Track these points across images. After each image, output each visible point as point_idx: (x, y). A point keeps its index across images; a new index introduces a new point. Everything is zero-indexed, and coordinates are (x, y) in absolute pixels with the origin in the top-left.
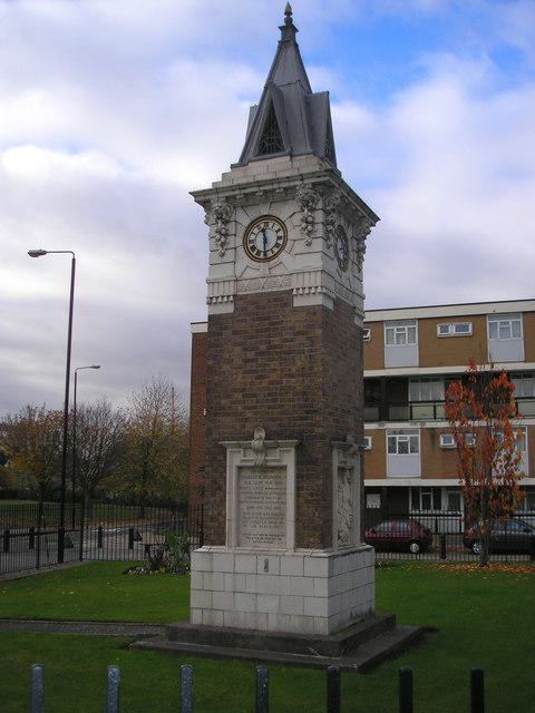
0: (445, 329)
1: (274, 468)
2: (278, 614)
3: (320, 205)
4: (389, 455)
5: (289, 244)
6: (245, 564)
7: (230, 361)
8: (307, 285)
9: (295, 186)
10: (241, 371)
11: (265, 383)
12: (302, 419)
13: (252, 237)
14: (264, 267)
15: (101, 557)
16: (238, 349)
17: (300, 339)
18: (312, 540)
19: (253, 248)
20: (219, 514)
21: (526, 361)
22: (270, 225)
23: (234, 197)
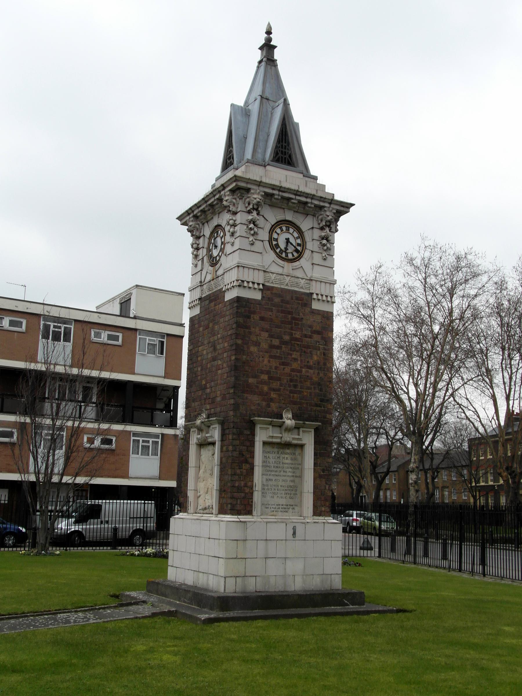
0: (98, 335)
1: (296, 446)
2: (303, 575)
4: (132, 456)
6: (278, 531)
7: (257, 344)
9: (324, 207)
10: (267, 355)
11: (287, 370)
12: (317, 405)
13: (275, 236)
14: (288, 267)
16: (265, 335)
17: (316, 337)
18: (323, 509)
19: (277, 246)
20: (246, 485)
23: (272, 195)
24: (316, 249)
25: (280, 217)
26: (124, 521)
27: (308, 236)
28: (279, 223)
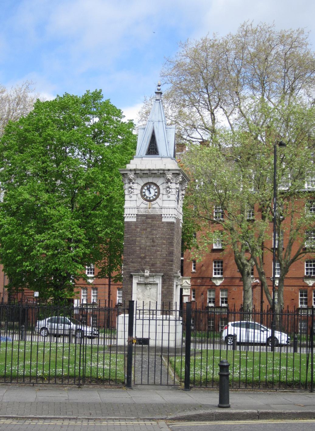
3: (174, 181)
5: (161, 195)
8: (171, 213)
13: (144, 191)
15: (56, 324)
21: (219, 407)
22: (152, 186)
24: (165, 193)
25: (145, 182)
26: (28, 356)
27: (161, 187)
28: (146, 184)
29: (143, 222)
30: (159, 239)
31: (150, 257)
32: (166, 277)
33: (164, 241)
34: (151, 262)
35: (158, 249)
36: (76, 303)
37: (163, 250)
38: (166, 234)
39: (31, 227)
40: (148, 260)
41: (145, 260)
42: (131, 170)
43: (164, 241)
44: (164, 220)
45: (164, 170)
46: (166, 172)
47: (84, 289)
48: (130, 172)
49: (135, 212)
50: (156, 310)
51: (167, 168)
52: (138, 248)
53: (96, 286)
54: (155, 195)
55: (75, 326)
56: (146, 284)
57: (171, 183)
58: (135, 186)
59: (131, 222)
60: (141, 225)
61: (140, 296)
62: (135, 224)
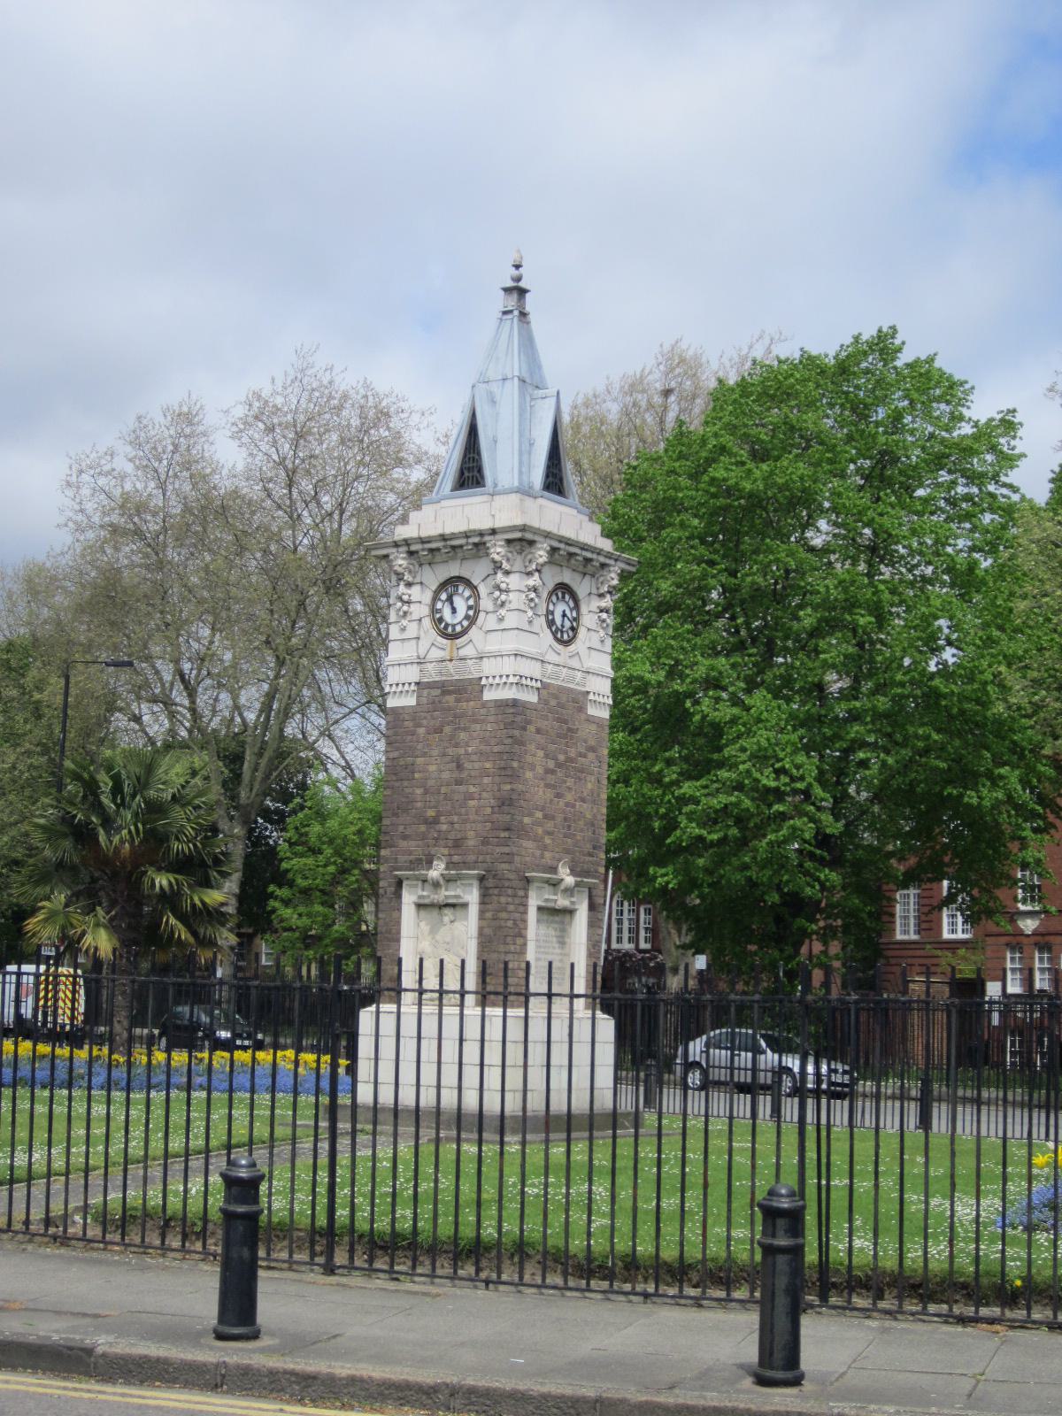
5: (482, 615)
8: (505, 672)
16: (541, 753)
22: (461, 589)
24: (490, 607)
25: (442, 578)
28: (443, 586)
29: (434, 706)
30: (474, 757)
31: (450, 819)
32: (490, 883)
33: (488, 765)
34: (452, 836)
35: (472, 789)
36: (993, 989)
37: (484, 795)
38: (493, 742)
39: (669, 762)
40: (444, 827)
41: (437, 827)
42: (396, 545)
43: (488, 765)
44: (488, 695)
45: (481, 534)
46: (487, 538)
47: (1013, 948)
48: (394, 550)
49: (412, 674)
50: (463, 993)
51: (486, 525)
52: (419, 791)
53: (1047, 938)
54: (467, 617)
55: (776, 1056)
56: (442, 906)
57: (507, 573)
58: (415, 592)
59: (403, 708)
60: (428, 715)
61: (426, 945)
62: (413, 713)
